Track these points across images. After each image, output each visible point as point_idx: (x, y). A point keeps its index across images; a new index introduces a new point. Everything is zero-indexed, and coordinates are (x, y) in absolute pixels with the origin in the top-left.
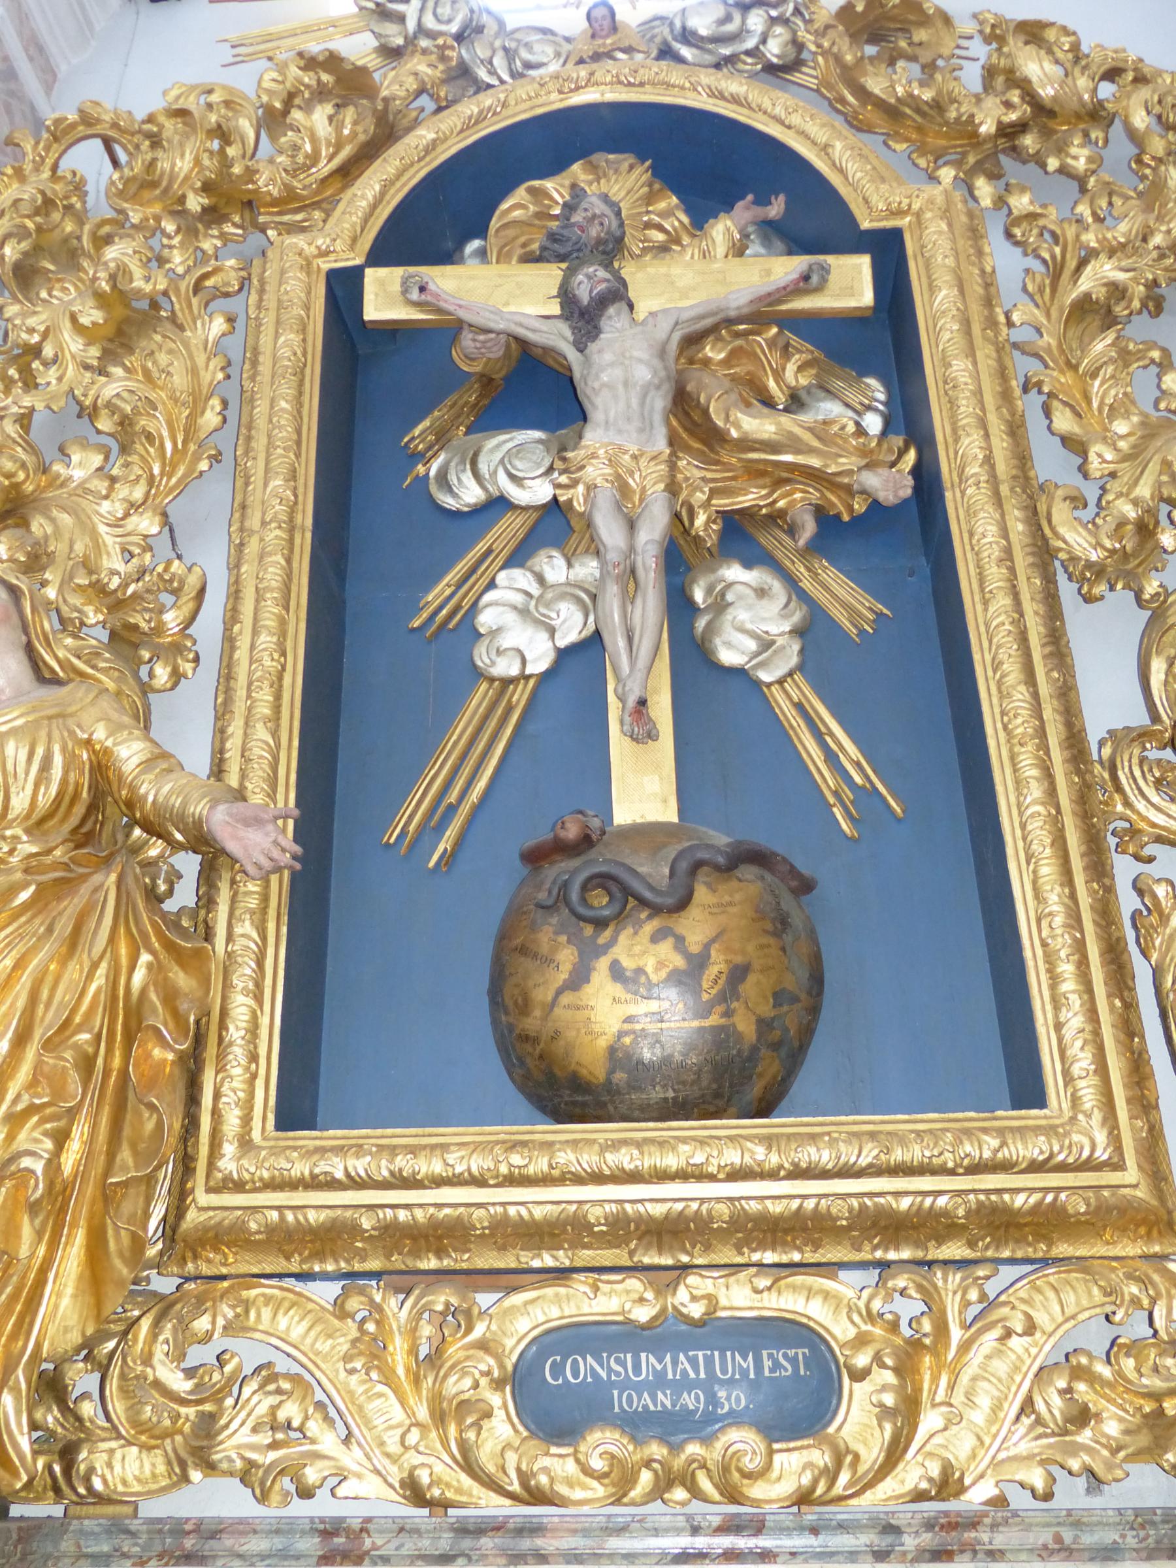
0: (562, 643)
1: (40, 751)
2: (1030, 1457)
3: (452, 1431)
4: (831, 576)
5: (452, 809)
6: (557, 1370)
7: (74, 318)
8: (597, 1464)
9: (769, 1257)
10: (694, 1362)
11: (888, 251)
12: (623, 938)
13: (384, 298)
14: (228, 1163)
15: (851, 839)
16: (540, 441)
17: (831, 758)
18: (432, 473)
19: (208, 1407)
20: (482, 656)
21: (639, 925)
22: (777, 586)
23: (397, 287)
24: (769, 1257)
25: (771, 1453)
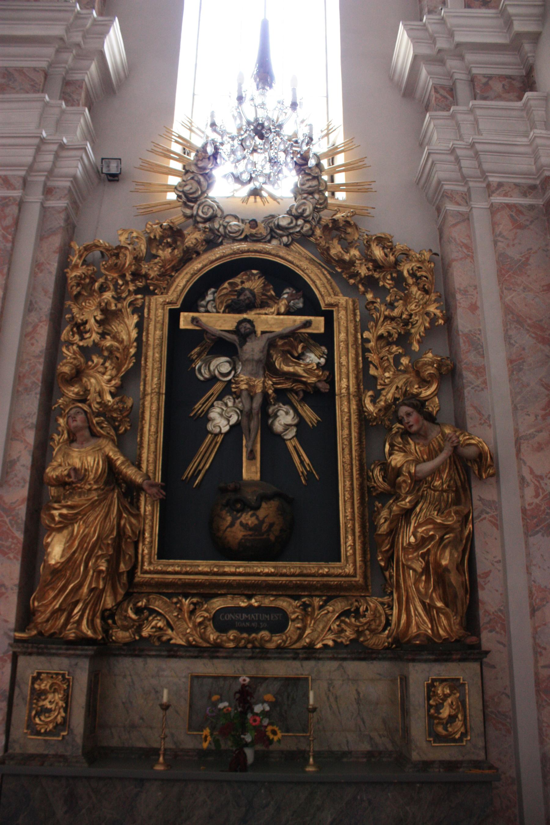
0: (231, 423)
1: (97, 460)
2: (330, 639)
3: (198, 629)
4: (307, 408)
5: (200, 471)
6: (223, 617)
7: (95, 317)
8: (231, 638)
9: (274, 593)
10: (255, 616)
11: (329, 317)
12: (244, 516)
13: (185, 321)
14: (146, 567)
15: (305, 486)
16: (227, 362)
17: (302, 462)
18: (197, 368)
19: (141, 623)
20: (210, 427)
21: (247, 513)
22: (291, 412)
23: (190, 319)
24: (274, 593)
25: (272, 637)
